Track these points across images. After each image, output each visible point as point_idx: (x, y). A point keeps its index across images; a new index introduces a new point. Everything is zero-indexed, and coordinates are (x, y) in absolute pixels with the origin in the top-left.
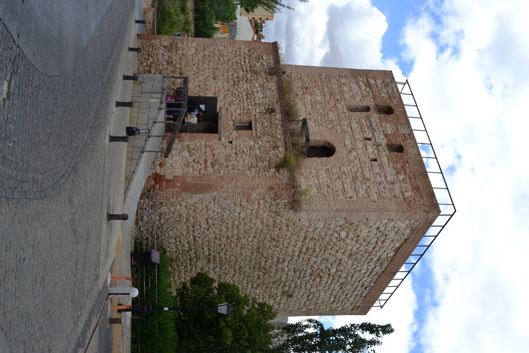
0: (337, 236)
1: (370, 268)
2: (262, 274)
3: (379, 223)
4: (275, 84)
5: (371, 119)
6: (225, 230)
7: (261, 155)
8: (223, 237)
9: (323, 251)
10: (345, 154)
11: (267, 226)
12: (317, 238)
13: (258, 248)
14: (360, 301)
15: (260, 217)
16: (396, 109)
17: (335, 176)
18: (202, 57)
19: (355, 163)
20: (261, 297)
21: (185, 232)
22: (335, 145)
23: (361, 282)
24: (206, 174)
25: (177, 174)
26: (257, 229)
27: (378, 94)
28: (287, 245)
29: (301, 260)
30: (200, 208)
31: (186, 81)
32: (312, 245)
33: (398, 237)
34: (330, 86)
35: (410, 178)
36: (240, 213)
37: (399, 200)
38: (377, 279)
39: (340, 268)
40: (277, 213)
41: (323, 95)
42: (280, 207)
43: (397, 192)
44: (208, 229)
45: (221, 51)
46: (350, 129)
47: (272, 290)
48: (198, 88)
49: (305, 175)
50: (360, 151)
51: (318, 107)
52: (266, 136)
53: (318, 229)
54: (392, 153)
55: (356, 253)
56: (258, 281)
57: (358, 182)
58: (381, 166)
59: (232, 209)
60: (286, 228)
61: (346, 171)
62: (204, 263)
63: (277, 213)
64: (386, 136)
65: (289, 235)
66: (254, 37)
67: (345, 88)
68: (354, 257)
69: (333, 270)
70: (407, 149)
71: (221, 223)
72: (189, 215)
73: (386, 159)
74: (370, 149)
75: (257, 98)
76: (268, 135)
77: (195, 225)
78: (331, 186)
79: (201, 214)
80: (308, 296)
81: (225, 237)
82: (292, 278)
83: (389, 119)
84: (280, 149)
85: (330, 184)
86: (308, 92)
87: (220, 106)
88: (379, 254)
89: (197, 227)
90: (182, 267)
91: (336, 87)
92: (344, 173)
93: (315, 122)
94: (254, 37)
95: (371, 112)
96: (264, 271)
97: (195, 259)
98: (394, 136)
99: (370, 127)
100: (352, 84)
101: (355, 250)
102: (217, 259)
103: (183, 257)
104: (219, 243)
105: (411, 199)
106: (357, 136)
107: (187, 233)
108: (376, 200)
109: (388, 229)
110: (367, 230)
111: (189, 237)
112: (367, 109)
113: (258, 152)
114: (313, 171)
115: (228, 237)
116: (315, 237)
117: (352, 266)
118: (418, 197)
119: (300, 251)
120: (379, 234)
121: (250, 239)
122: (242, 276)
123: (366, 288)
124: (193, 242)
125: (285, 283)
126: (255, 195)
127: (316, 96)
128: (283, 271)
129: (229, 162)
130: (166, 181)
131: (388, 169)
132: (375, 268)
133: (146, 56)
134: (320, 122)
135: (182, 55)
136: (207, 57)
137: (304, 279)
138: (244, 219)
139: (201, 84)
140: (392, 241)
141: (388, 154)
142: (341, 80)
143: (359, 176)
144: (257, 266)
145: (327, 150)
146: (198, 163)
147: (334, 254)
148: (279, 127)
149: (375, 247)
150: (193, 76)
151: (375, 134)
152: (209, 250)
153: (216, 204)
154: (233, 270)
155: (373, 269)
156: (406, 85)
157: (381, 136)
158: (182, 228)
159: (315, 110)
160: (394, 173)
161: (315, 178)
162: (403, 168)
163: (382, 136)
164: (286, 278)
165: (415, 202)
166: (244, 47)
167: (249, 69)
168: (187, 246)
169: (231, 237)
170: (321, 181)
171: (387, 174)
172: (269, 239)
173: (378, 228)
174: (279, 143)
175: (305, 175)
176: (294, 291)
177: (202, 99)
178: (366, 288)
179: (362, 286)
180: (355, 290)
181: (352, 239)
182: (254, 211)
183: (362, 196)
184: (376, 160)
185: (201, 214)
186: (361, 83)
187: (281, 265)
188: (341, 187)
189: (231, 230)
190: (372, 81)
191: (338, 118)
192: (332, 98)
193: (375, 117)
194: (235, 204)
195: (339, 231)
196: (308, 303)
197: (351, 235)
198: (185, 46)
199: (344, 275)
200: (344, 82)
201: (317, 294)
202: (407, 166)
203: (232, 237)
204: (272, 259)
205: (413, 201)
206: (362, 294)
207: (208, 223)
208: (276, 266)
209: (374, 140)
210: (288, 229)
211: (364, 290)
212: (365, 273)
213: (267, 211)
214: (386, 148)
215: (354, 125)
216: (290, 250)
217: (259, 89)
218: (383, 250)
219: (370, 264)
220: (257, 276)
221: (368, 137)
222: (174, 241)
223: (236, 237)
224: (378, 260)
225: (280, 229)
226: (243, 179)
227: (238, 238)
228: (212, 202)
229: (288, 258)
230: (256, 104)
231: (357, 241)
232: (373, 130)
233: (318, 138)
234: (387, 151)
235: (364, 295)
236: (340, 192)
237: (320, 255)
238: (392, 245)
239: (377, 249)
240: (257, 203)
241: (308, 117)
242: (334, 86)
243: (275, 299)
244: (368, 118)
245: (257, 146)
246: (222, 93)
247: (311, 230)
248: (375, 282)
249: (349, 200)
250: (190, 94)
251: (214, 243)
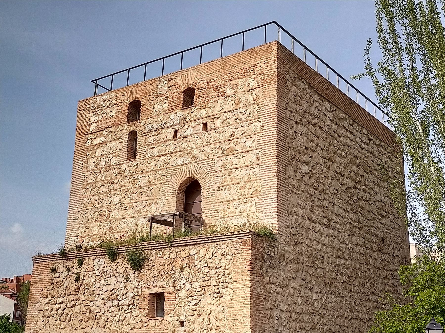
0: (307, 177)
2: (358, 280)
3: (290, 122)
5: (147, 130)
7: (201, 280)
9: (326, 196)
11: (297, 271)
12: (311, 203)
14: (386, 147)
15: (286, 282)
16: (134, 96)
17: (228, 178)
19: (209, 151)
20: (386, 281)
23: (362, 146)
29: (338, 226)
32: (318, 211)
33: (307, 98)
34: (98, 185)
35: (230, 80)
36: (281, 310)
37: (260, 95)
38: (359, 124)
39: (346, 173)
40: (281, 258)
41: (112, 194)
42: (272, 254)
43: (249, 97)
46: (162, 158)
50: (192, 145)
52: (173, 272)
54: (195, 103)
55: (328, 151)
56: (367, 285)
57: (236, 148)
58: (213, 118)
59: (276, 321)
60: (300, 246)
61: (221, 163)
63: (281, 258)
64: (171, 110)
68: (332, 155)
69: (350, 182)
70: (189, 83)
73: (204, 111)
74: (190, 131)
75: (117, 286)
78: (242, 183)
80: (383, 217)
82: (361, 239)
83: (148, 106)
85: (239, 186)
92: (223, 166)
93: (150, 204)
95: (137, 130)
96: (354, 277)
98: (171, 99)
101: (323, 154)
105: (258, 79)
110: (299, 138)
112: (133, 136)
114: (220, 208)
116: (309, 206)
117: (344, 157)
118: (256, 69)
119: (327, 226)
120: (304, 122)
123: (370, 140)
125: (367, 248)
128: (351, 251)
131: (218, 109)
132: (345, 127)
134: (151, 197)
138: (289, 305)
142: (90, 168)
144: (348, 286)
145: (191, 190)
147: (329, 181)
149: (320, 127)
151: (169, 124)
154: (354, 321)
155: (347, 130)
157: (172, 117)
160: (222, 100)
161: (231, 205)
162: (216, 88)
164: (361, 246)
165: (263, 74)
172: (314, 269)
173: (297, 123)
174: (184, 255)
178: (370, 140)
179: (367, 144)
180: (372, 153)
182: (279, 290)
184: (205, 125)
186: (96, 142)
187: (345, 254)
191: (146, 173)
192: (116, 181)
193: (143, 124)
194: (271, 317)
195: (301, 174)
196: (391, 216)
197: (305, 158)
199: (355, 168)
200: (94, 164)
201: (380, 205)
202: (214, 83)
203: (312, 322)
204: (338, 265)
206: (377, 145)
210: (301, 243)
211: (372, 142)
212: (352, 140)
214: (188, 111)
215: (155, 152)
217: (103, 282)
218: (324, 118)
219: (340, 133)
221: (173, 133)
223: (312, 316)
224: (335, 124)
225: (301, 254)
227: (313, 313)
229: (336, 243)
231: (313, 151)
234: (193, 109)
235: (378, 142)
236: (251, 172)
237: (331, 200)
238: (317, 104)
241: (143, 213)
242: (99, 178)
244: (146, 134)
245: (188, 286)
248: (362, 127)
249: (261, 160)
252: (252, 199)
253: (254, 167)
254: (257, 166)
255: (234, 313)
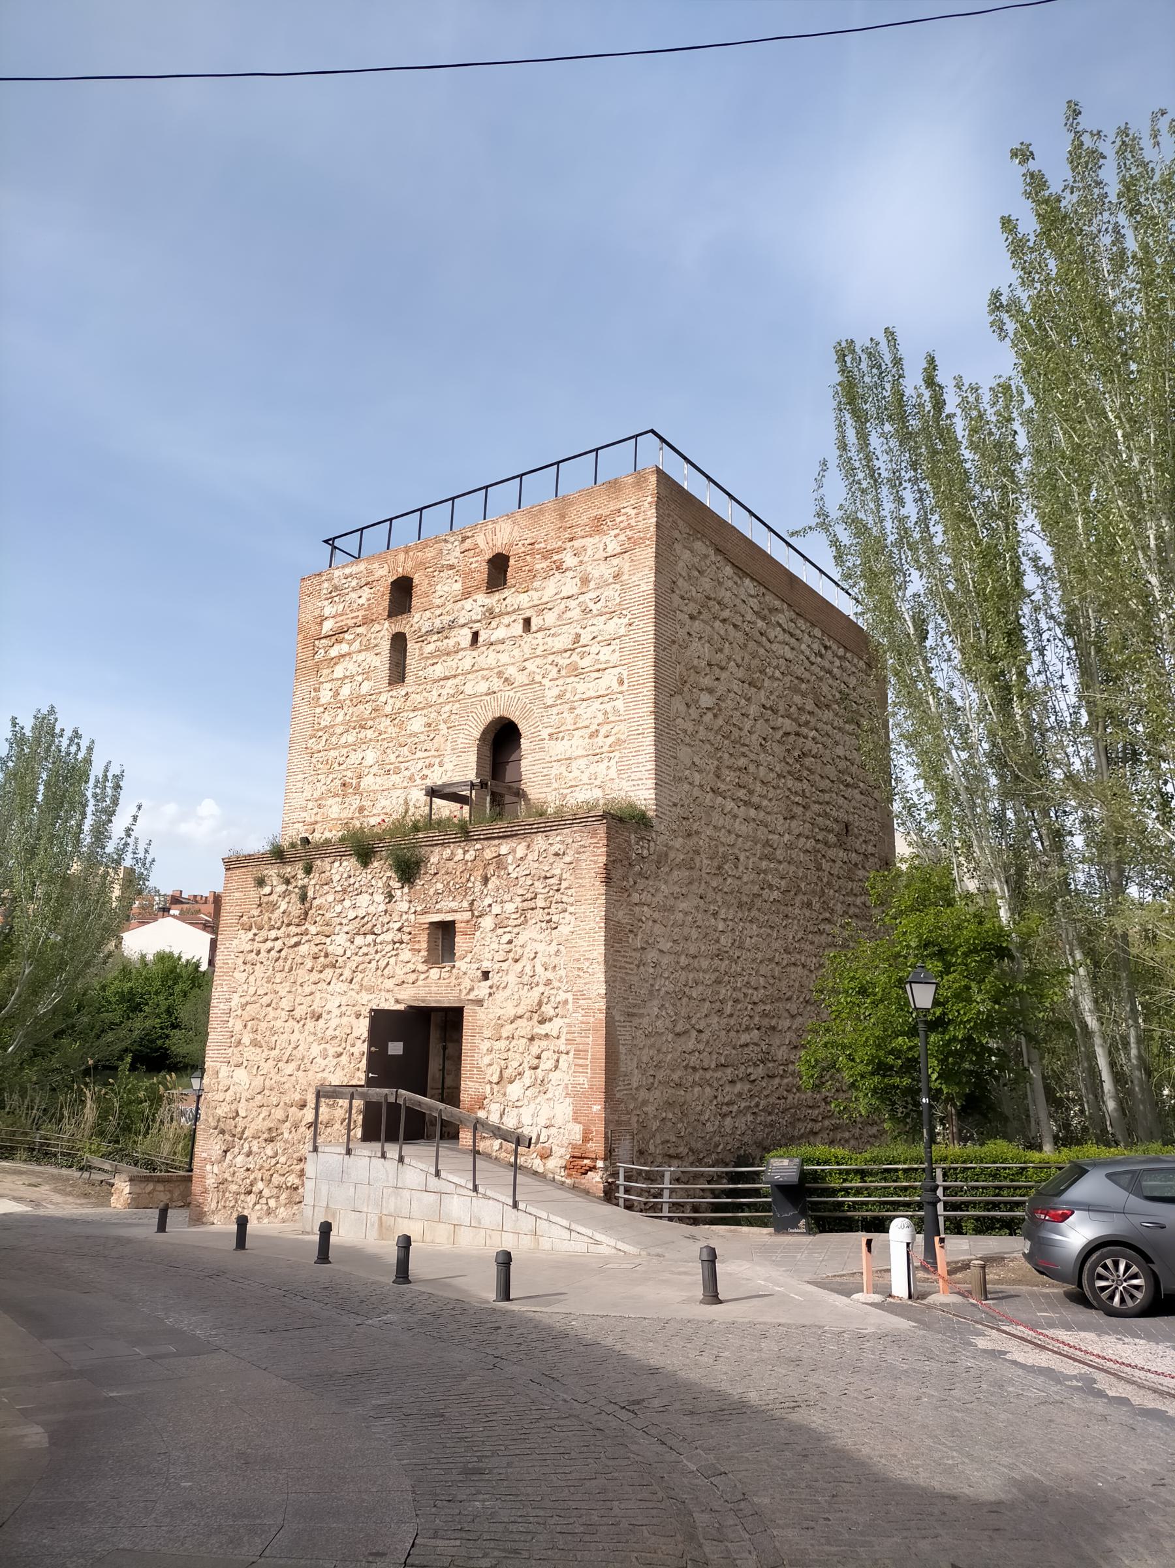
0: (710, 715)
1: (781, 636)
4: (337, 864)
5: (424, 631)
6: (701, 988)
7: (519, 899)
8: (718, 993)
9: (744, 749)
10: (511, 693)
12: (716, 763)
13: (740, 905)
14: (856, 660)
15: (671, 902)
16: (400, 570)
17: (569, 718)
18: (259, 1050)
20: (850, 899)
21: (708, 1090)
22: (490, 719)
23: (813, 659)
24: (569, 1037)
25: (569, 1111)
26: (697, 908)
27: (361, 613)
28: (733, 836)
29: (765, 803)
30: (651, 1053)
31: (324, 1093)
32: (730, 776)
34: (339, 730)
35: (571, 540)
38: (806, 620)
39: (782, 708)
41: (364, 746)
43: (601, 571)
44: (700, 1031)
45: (243, 1000)
46: (450, 682)
47: (835, 872)
48: (344, 1059)
49: (565, 792)
51: (392, 758)
52: (470, 885)
53: (696, 760)
54: (510, 582)
56: (817, 906)
57: (582, 663)
60: (695, 839)
61: (555, 692)
62: (778, 1043)
64: (466, 595)
65: (709, 831)
66: (174, 916)
67: (345, 691)
70: (499, 544)
71: (685, 1000)
72: (665, 1083)
75: (372, 909)
76: (468, 880)
77: (692, 1064)
78: (594, 728)
79: (664, 1050)
80: (847, 786)
81: (716, 987)
84: (504, 849)
85: (588, 731)
86: (354, 782)
87: (392, 1001)
88: (750, 616)
89: (693, 1060)
90: (790, 1097)
91: (341, 713)
92: (559, 697)
93: (431, 766)
94: (174, 916)
95: (406, 630)
97: (770, 1065)
98: (468, 574)
99: (445, 634)
100: (335, 676)
101: (740, 673)
102: (768, 1007)
103: (767, 1096)
104: (730, 1003)
105: (622, 537)
106: (467, 664)
107: (710, 1085)
108: (626, 621)
109: (694, 594)
111: (718, 1079)
113: (510, 907)
115: (718, 982)
116: (712, 768)
119: (746, 803)
120: (706, 615)
121: (721, 926)
122: (807, 947)
123: (826, 647)
124: (729, 1071)
126: (621, 913)
127: (365, 763)
129: (537, 978)
130: (586, 1139)
132: (780, 625)
133: (252, 1199)
134: (433, 753)
135: (251, 1103)
136: (259, 1037)
137: (808, 795)
139: (331, 1051)
140: (719, 583)
141: (513, 590)
142: (323, 701)
143: (568, 661)
144: (782, 908)
145: (502, 739)
146: (539, 1057)
147: (751, 722)
148: (447, 852)
149: (735, 626)
150: (310, 1073)
151: (462, 621)
152: (747, 1029)
153: (641, 1011)
154: (792, 969)
155: (784, 630)
156: (337, 543)
158: (698, 1099)
159: (402, 766)
160: (558, 576)
162: (547, 554)
163: (468, 604)
164: (807, 838)
165: (629, 527)
166: (236, 942)
167: (293, 929)
168: (739, 1087)
169: (717, 974)
170: (582, 752)
171: (561, 596)
172: (720, 879)
173: (692, 617)
174: (489, 854)
175: (565, 792)
176: (836, 821)
177: (373, 1049)
178: (826, 647)
179: (821, 656)
181: (717, 679)
182: (656, 915)
183: (617, 654)
184: (527, 622)
185: (664, 1050)
186: (334, 652)
187: (778, 852)
188: (596, 704)
189: (701, 974)
190: (328, 626)
191: (422, 709)
192: (370, 723)
196: (862, 784)
197: (707, 681)
198: (229, 1096)
199: (797, 699)
201: (843, 764)
202: (543, 545)
204: (765, 872)
205: (629, 533)
206: (839, 658)
207: (686, 1032)
208: (780, 862)
209: (478, 624)
210: (697, 833)
211: (830, 652)
212: (793, 649)
213: (657, 883)
215: (439, 670)
216: (744, 828)
217: (347, 903)
218: (742, 608)
219: (771, 636)
220: (805, 910)
222: (728, 1120)
223: (716, 961)
224: (764, 619)
226: (580, 942)
228: (636, 1021)
229: (762, 833)
230: (386, 911)
231: (722, 669)
232: (452, 626)
233: (472, 758)
235: (841, 652)
236: (608, 707)
237: (753, 756)
238: (730, 584)
239: (738, 620)
240: (637, 909)
241: (419, 782)
242: (340, 719)
243: (856, 865)
244: (422, 639)
245: (496, 909)
246: (358, 997)
247: (697, 778)
248: (813, 625)
249: (626, 685)
250: (360, 1078)
251: (731, 1015)
252: (612, 755)
253: (614, 697)
254: (619, 696)
255: (577, 956)
